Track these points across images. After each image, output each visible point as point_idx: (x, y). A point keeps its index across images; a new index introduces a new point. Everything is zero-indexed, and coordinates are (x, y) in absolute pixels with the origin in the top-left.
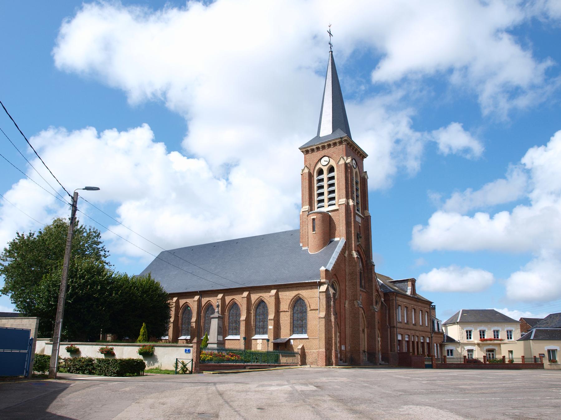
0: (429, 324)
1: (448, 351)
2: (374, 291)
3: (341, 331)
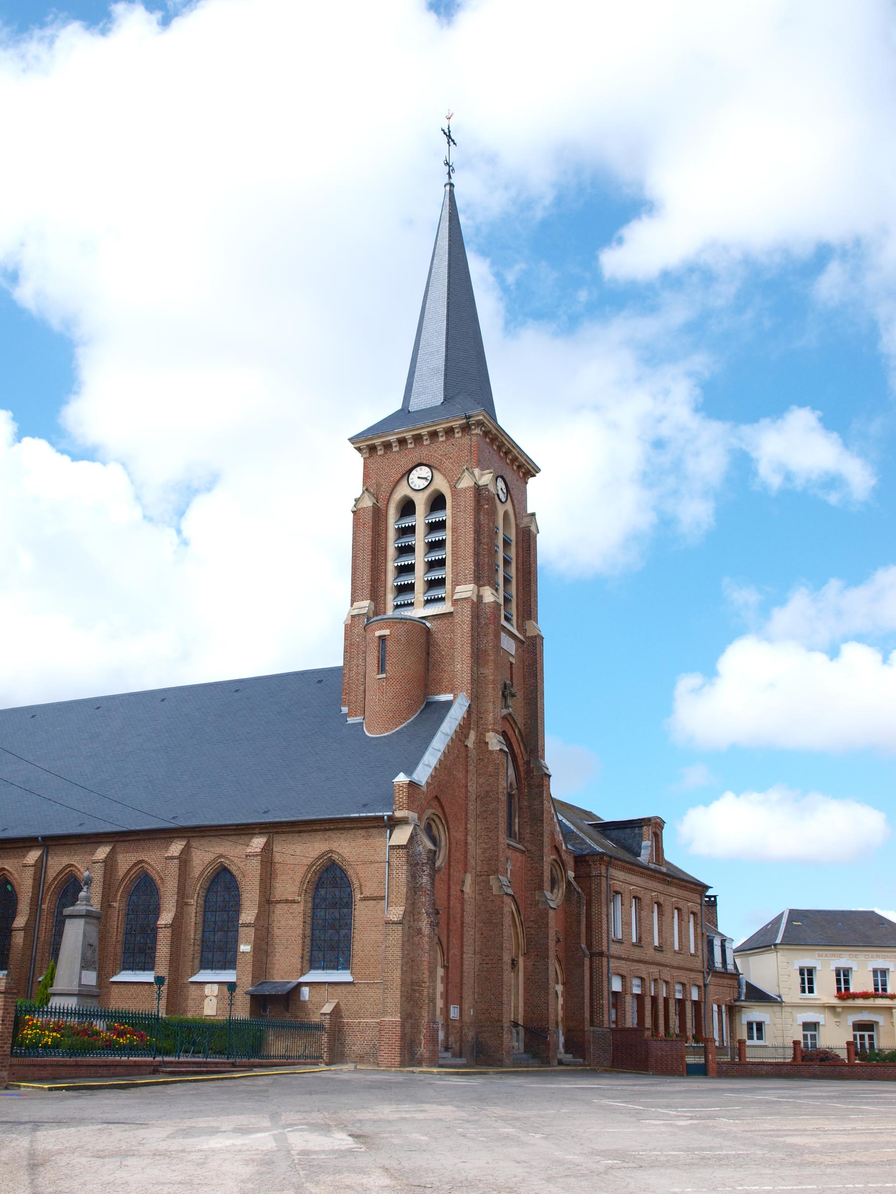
0: (700, 947)
1: (750, 1024)
2: (547, 848)
3: (448, 960)
